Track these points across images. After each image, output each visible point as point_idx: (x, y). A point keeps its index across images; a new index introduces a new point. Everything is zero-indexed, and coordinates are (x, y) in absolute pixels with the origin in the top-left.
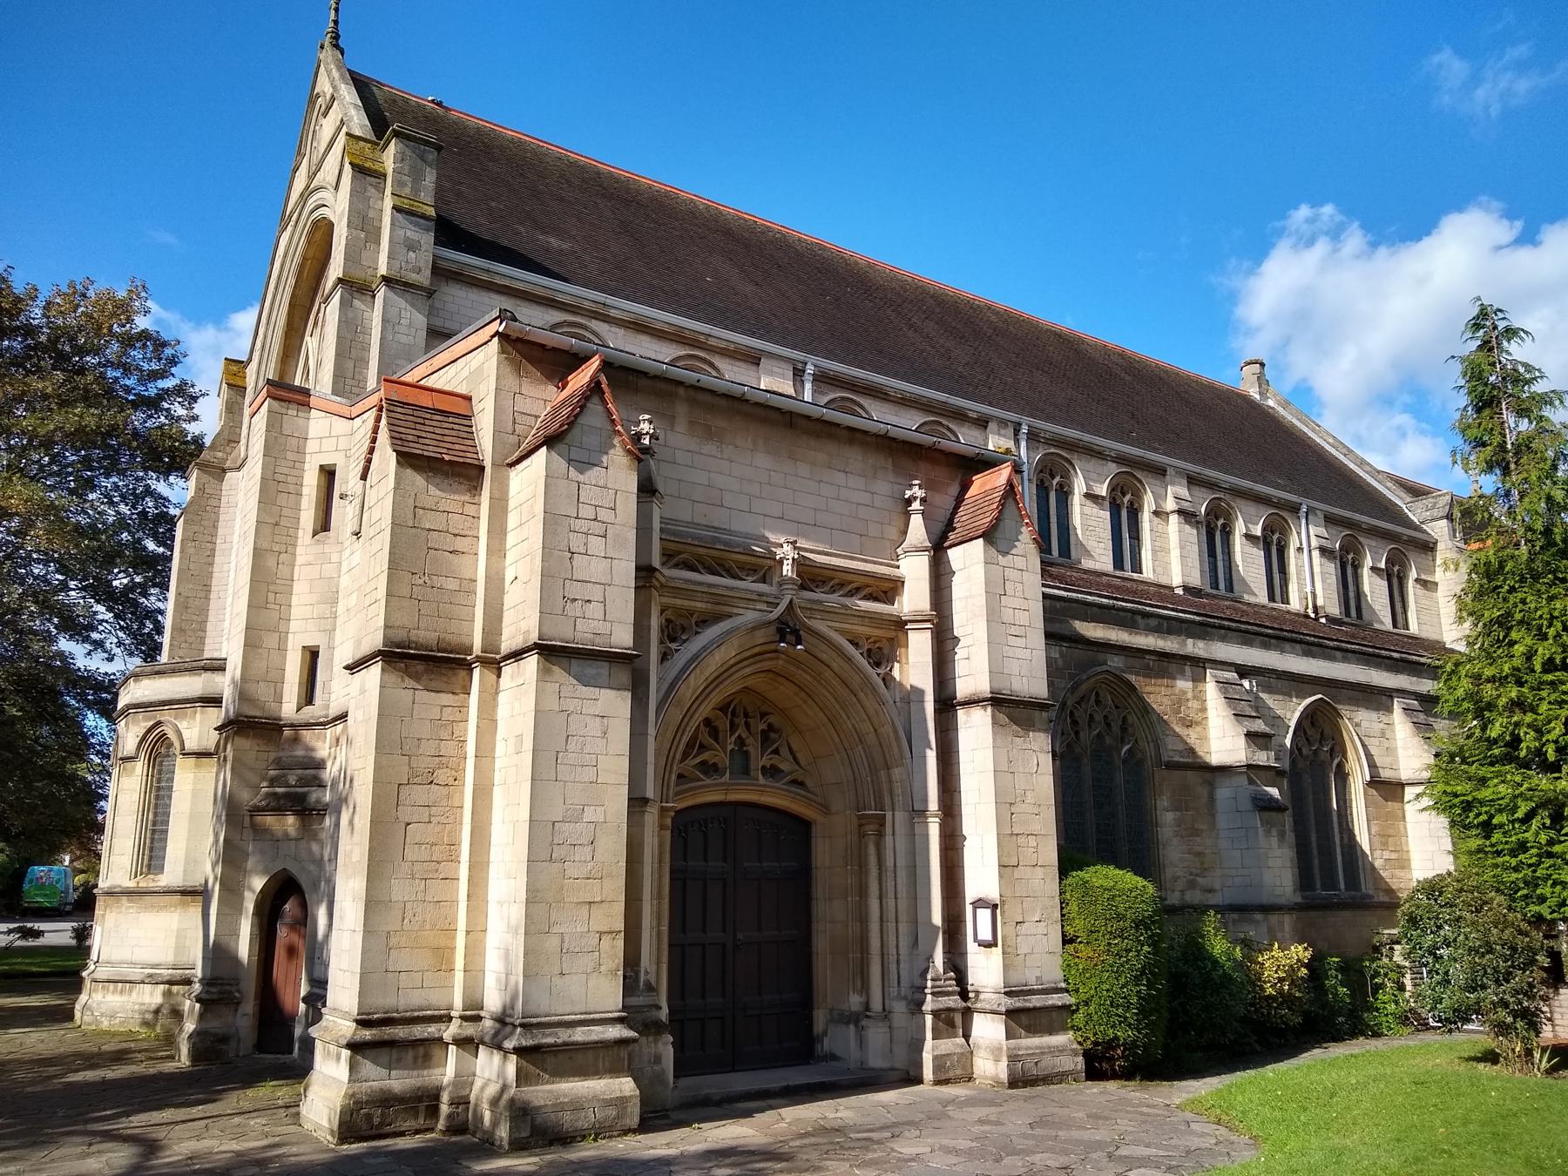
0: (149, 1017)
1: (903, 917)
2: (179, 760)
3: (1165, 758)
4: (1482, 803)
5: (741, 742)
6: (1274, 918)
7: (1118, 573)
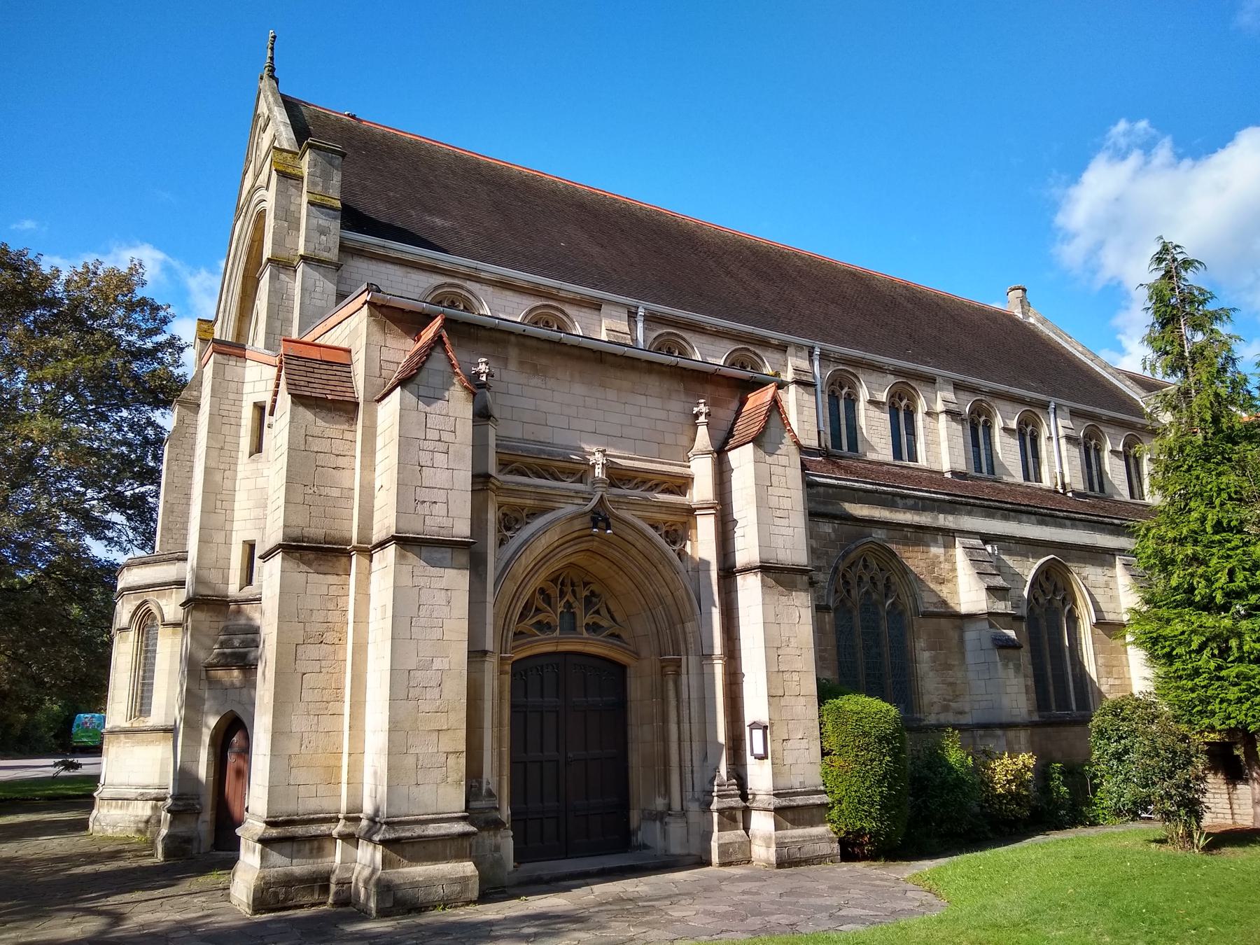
0: (142, 825)
1: (696, 737)
2: (161, 629)
3: (922, 609)
4: (1166, 639)
5: (569, 605)
6: (1011, 734)
7: (897, 463)
